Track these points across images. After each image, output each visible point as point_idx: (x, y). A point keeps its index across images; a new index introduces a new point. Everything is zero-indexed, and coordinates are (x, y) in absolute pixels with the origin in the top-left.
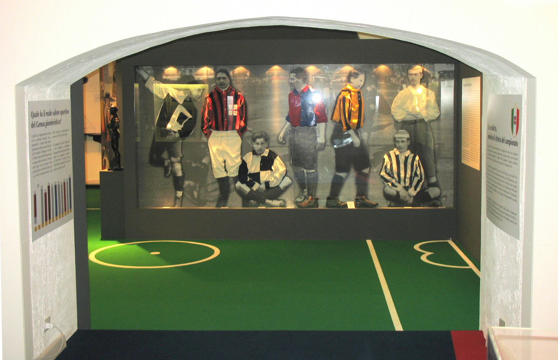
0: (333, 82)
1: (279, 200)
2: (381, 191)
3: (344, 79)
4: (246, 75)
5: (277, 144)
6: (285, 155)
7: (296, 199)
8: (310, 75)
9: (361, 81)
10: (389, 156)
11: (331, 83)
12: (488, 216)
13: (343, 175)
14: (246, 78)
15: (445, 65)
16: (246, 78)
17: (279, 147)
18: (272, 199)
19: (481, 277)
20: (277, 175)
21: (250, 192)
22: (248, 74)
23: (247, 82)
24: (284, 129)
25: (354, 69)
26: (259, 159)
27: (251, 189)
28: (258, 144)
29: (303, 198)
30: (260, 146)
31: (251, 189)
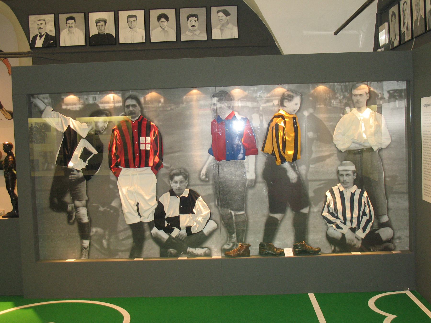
1: (203, 248)
2: (324, 234)
4: (160, 102)
5: (198, 182)
9: (296, 104)
13: (278, 216)
14: (160, 105)
17: (201, 185)
18: (195, 246)
20: (200, 219)
22: (162, 100)
23: (161, 109)
26: (178, 200)
27: (170, 236)
28: (176, 182)
29: (231, 244)
30: (178, 185)
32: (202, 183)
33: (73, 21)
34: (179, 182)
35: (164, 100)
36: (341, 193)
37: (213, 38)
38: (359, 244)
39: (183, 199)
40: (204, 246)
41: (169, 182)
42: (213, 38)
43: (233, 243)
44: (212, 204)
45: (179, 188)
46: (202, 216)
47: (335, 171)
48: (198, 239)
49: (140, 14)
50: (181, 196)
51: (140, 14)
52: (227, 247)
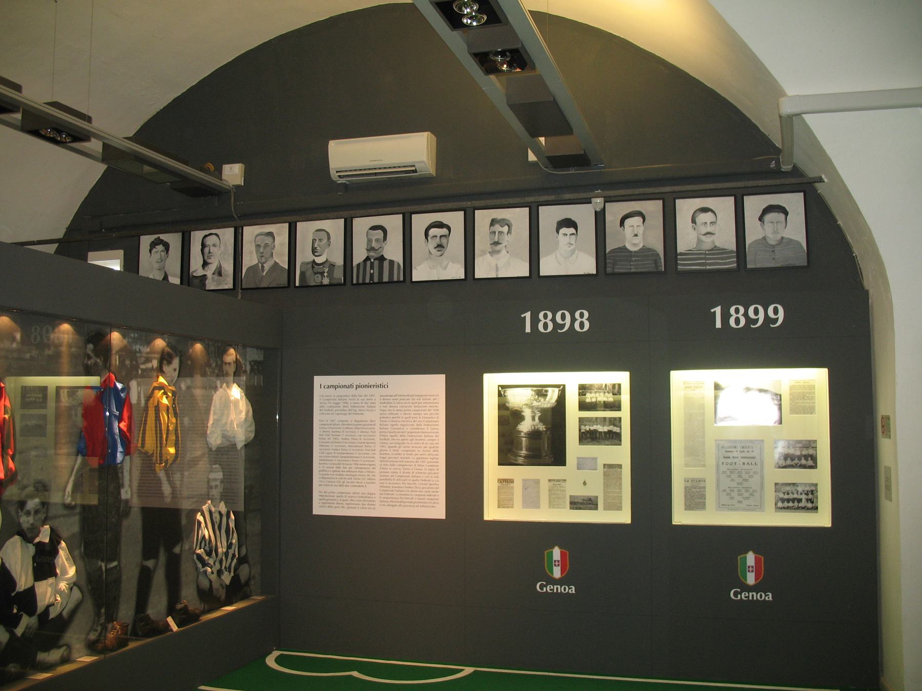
0: (142, 370)
1: (61, 647)
2: (194, 586)
3: (155, 363)
4: (14, 339)
5: (62, 511)
6: (74, 535)
7: (88, 634)
8: (114, 352)
9: (175, 370)
10: (203, 515)
11: (140, 372)
12: (658, 255)
13: (150, 563)
14: (14, 345)
15: (163, 488)
16: (14, 345)
17: (64, 516)
18: (47, 648)
19: (871, 292)
20: (63, 585)
21: (10, 640)
22: (18, 336)
23: (15, 355)
24: (73, 478)
25: (168, 345)
26: (32, 549)
27: (12, 634)
28: (28, 513)
29: (99, 629)
30: (31, 519)
31: (12, 634)
32: (66, 512)
33: (572, 230)
34: (32, 513)
35: (21, 337)
36: (211, 512)
37: (478, 275)
38: (222, 594)
39: (40, 546)
40: (62, 642)
41: (18, 513)
42: (478, 275)
43: (101, 625)
44: (77, 553)
45: (32, 525)
46: (67, 580)
47: (206, 480)
48: (53, 629)
49: (455, 219)
50: (37, 540)
51: (455, 219)
52: (93, 636)
